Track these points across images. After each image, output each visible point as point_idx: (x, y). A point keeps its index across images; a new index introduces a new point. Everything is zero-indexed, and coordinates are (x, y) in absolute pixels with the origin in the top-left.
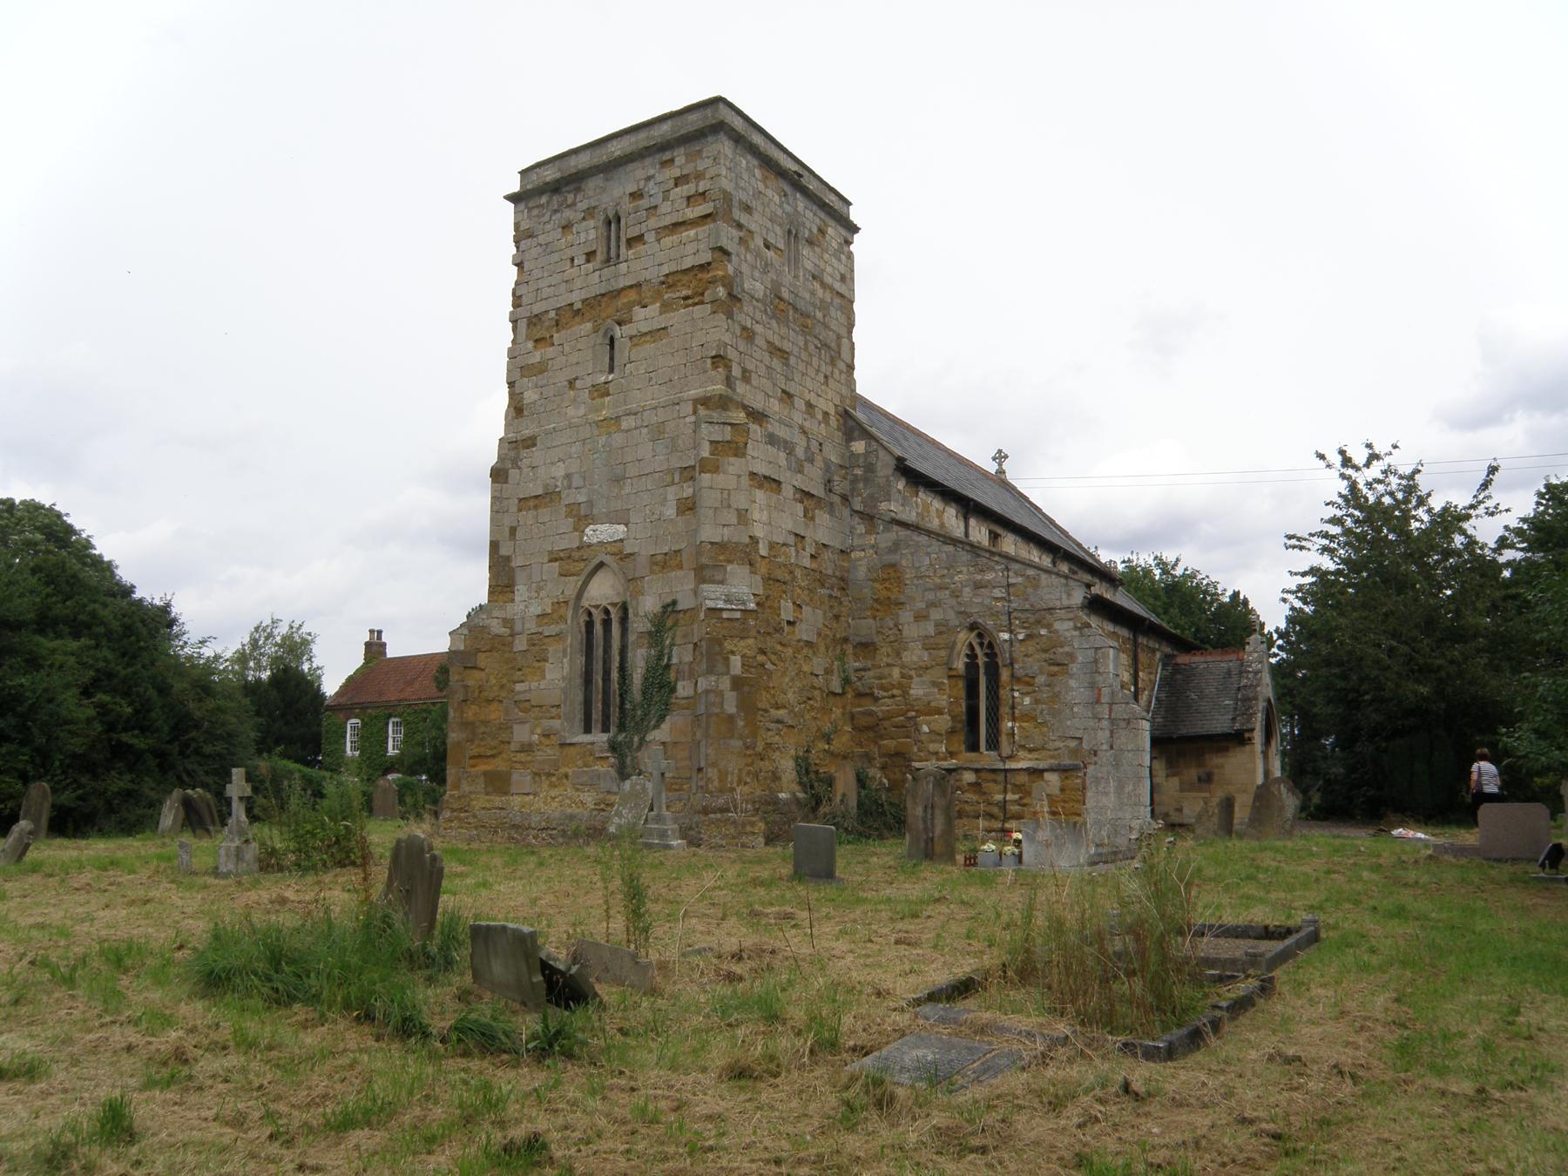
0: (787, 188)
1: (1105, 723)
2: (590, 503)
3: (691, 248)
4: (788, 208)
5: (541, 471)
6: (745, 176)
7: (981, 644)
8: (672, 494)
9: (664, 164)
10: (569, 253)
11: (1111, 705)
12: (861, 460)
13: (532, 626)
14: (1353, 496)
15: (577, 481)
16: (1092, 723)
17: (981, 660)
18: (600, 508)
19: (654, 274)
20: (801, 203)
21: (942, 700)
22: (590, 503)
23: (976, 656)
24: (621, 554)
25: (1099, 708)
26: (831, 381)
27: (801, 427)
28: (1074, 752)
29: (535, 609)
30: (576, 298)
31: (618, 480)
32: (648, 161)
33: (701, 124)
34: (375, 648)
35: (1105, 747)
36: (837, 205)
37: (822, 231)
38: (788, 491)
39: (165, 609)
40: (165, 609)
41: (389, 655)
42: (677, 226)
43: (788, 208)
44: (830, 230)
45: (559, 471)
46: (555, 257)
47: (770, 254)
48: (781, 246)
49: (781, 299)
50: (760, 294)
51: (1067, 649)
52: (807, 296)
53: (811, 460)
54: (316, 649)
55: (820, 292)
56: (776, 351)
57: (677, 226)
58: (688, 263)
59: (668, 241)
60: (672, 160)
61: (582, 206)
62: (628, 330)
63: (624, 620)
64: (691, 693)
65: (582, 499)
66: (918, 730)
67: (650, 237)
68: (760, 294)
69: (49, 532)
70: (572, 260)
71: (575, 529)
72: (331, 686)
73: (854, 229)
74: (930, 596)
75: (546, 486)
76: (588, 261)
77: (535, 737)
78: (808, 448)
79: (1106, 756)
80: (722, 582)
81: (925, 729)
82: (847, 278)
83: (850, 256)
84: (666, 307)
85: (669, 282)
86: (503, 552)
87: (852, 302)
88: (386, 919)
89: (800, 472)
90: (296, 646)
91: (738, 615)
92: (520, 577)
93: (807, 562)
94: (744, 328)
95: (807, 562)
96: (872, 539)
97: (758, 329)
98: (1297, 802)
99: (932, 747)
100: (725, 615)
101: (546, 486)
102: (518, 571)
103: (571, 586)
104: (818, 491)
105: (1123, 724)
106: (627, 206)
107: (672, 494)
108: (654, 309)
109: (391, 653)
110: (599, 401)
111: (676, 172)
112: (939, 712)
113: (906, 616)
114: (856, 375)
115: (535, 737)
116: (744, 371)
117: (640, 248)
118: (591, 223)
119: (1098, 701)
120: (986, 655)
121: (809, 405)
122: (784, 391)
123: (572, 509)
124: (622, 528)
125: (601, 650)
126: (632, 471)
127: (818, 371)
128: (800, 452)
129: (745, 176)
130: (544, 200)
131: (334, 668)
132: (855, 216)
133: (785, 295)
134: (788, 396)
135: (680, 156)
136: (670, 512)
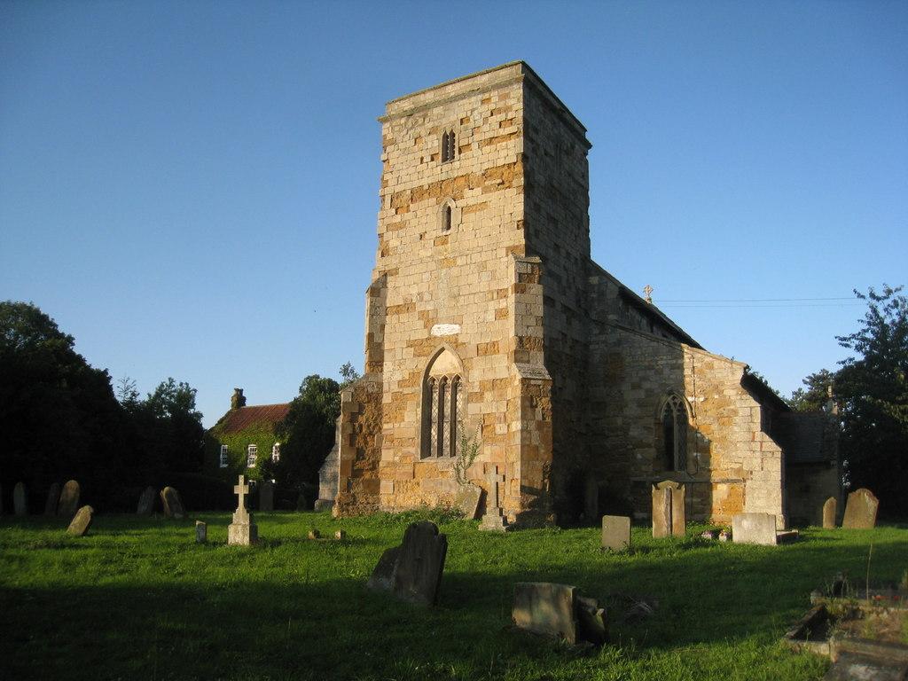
0: (556, 120)
1: (758, 454)
2: (436, 311)
3: (503, 153)
4: (556, 132)
5: (402, 289)
6: (534, 110)
7: (675, 404)
8: (493, 306)
9: (483, 102)
10: (420, 154)
11: (761, 443)
12: (596, 288)
13: (395, 388)
14: (875, 319)
15: (427, 297)
16: (749, 453)
17: (675, 414)
18: (442, 314)
19: (478, 170)
20: (563, 130)
21: (651, 439)
22: (436, 311)
23: (672, 411)
24: (456, 344)
25: (753, 444)
26: (578, 238)
27: (564, 267)
28: (739, 471)
29: (398, 377)
30: (425, 182)
31: (455, 297)
32: (473, 99)
33: (508, 78)
34: (239, 399)
35: (757, 469)
36: (580, 130)
37: (573, 147)
38: (558, 307)
39: (106, 372)
40: (106, 372)
41: (247, 405)
42: (491, 141)
43: (556, 132)
44: (577, 146)
45: (414, 291)
46: (410, 157)
47: (548, 159)
48: (553, 154)
49: (553, 187)
50: (542, 184)
51: (732, 407)
52: (566, 186)
53: (570, 288)
54: (197, 400)
55: (572, 184)
56: (552, 220)
57: (491, 141)
58: (501, 162)
59: (487, 149)
60: (489, 99)
61: (429, 125)
62: (461, 203)
63: (455, 387)
64: (506, 431)
65: (429, 307)
66: (635, 458)
67: (475, 146)
68: (542, 184)
69: (38, 322)
70: (422, 159)
71: (425, 327)
72: (208, 423)
73: (589, 146)
74: (641, 374)
75: (405, 300)
76: (432, 160)
77: (397, 459)
78: (568, 280)
79: (757, 475)
80: (528, 362)
81: (639, 456)
82: (585, 176)
83: (587, 162)
84: (486, 190)
85: (486, 175)
86: (377, 340)
87: (588, 190)
88: (53, 564)
89: (565, 295)
90: (186, 398)
91: (540, 382)
92: (387, 356)
93: (567, 351)
94: (535, 204)
95: (567, 351)
96: (603, 338)
97: (543, 205)
98: (876, 505)
99: (644, 468)
100: (533, 382)
101: (405, 300)
102: (385, 353)
103: (422, 363)
104: (572, 306)
105: (770, 455)
106: (458, 128)
107: (493, 306)
108: (478, 191)
109: (249, 404)
110: (441, 247)
111: (492, 106)
112: (649, 446)
113: (626, 387)
114: (590, 235)
115: (397, 459)
116: (536, 230)
117: (469, 153)
118: (435, 136)
119: (753, 440)
120: (679, 410)
121: (568, 253)
122: (555, 244)
123: (423, 315)
124: (457, 327)
125: (449, 404)
126: (465, 291)
127: (572, 232)
128: (564, 283)
129: (534, 110)
130: (403, 121)
131: (211, 411)
132: (588, 136)
133: (556, 185)
134: (557, 247)
135: (494, 95)
136: (491, 317)
